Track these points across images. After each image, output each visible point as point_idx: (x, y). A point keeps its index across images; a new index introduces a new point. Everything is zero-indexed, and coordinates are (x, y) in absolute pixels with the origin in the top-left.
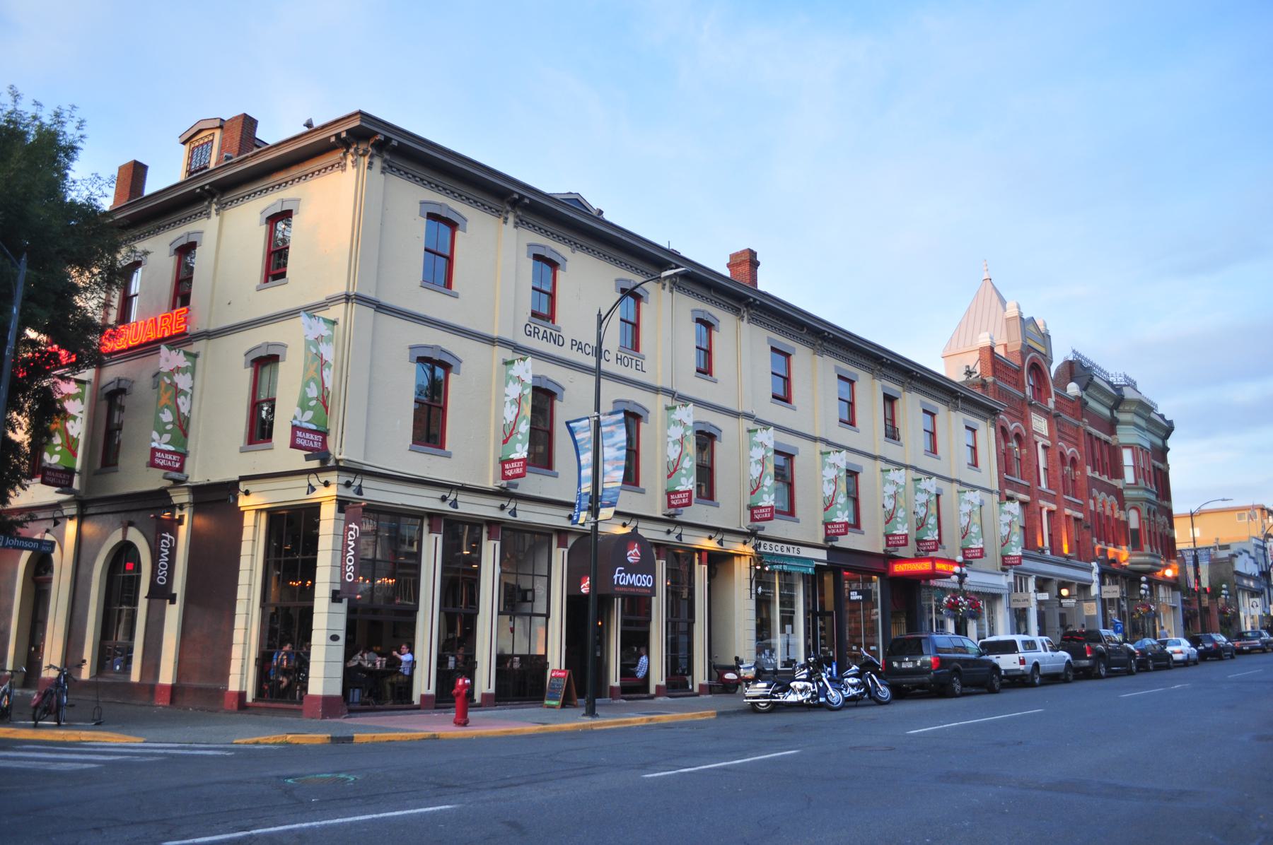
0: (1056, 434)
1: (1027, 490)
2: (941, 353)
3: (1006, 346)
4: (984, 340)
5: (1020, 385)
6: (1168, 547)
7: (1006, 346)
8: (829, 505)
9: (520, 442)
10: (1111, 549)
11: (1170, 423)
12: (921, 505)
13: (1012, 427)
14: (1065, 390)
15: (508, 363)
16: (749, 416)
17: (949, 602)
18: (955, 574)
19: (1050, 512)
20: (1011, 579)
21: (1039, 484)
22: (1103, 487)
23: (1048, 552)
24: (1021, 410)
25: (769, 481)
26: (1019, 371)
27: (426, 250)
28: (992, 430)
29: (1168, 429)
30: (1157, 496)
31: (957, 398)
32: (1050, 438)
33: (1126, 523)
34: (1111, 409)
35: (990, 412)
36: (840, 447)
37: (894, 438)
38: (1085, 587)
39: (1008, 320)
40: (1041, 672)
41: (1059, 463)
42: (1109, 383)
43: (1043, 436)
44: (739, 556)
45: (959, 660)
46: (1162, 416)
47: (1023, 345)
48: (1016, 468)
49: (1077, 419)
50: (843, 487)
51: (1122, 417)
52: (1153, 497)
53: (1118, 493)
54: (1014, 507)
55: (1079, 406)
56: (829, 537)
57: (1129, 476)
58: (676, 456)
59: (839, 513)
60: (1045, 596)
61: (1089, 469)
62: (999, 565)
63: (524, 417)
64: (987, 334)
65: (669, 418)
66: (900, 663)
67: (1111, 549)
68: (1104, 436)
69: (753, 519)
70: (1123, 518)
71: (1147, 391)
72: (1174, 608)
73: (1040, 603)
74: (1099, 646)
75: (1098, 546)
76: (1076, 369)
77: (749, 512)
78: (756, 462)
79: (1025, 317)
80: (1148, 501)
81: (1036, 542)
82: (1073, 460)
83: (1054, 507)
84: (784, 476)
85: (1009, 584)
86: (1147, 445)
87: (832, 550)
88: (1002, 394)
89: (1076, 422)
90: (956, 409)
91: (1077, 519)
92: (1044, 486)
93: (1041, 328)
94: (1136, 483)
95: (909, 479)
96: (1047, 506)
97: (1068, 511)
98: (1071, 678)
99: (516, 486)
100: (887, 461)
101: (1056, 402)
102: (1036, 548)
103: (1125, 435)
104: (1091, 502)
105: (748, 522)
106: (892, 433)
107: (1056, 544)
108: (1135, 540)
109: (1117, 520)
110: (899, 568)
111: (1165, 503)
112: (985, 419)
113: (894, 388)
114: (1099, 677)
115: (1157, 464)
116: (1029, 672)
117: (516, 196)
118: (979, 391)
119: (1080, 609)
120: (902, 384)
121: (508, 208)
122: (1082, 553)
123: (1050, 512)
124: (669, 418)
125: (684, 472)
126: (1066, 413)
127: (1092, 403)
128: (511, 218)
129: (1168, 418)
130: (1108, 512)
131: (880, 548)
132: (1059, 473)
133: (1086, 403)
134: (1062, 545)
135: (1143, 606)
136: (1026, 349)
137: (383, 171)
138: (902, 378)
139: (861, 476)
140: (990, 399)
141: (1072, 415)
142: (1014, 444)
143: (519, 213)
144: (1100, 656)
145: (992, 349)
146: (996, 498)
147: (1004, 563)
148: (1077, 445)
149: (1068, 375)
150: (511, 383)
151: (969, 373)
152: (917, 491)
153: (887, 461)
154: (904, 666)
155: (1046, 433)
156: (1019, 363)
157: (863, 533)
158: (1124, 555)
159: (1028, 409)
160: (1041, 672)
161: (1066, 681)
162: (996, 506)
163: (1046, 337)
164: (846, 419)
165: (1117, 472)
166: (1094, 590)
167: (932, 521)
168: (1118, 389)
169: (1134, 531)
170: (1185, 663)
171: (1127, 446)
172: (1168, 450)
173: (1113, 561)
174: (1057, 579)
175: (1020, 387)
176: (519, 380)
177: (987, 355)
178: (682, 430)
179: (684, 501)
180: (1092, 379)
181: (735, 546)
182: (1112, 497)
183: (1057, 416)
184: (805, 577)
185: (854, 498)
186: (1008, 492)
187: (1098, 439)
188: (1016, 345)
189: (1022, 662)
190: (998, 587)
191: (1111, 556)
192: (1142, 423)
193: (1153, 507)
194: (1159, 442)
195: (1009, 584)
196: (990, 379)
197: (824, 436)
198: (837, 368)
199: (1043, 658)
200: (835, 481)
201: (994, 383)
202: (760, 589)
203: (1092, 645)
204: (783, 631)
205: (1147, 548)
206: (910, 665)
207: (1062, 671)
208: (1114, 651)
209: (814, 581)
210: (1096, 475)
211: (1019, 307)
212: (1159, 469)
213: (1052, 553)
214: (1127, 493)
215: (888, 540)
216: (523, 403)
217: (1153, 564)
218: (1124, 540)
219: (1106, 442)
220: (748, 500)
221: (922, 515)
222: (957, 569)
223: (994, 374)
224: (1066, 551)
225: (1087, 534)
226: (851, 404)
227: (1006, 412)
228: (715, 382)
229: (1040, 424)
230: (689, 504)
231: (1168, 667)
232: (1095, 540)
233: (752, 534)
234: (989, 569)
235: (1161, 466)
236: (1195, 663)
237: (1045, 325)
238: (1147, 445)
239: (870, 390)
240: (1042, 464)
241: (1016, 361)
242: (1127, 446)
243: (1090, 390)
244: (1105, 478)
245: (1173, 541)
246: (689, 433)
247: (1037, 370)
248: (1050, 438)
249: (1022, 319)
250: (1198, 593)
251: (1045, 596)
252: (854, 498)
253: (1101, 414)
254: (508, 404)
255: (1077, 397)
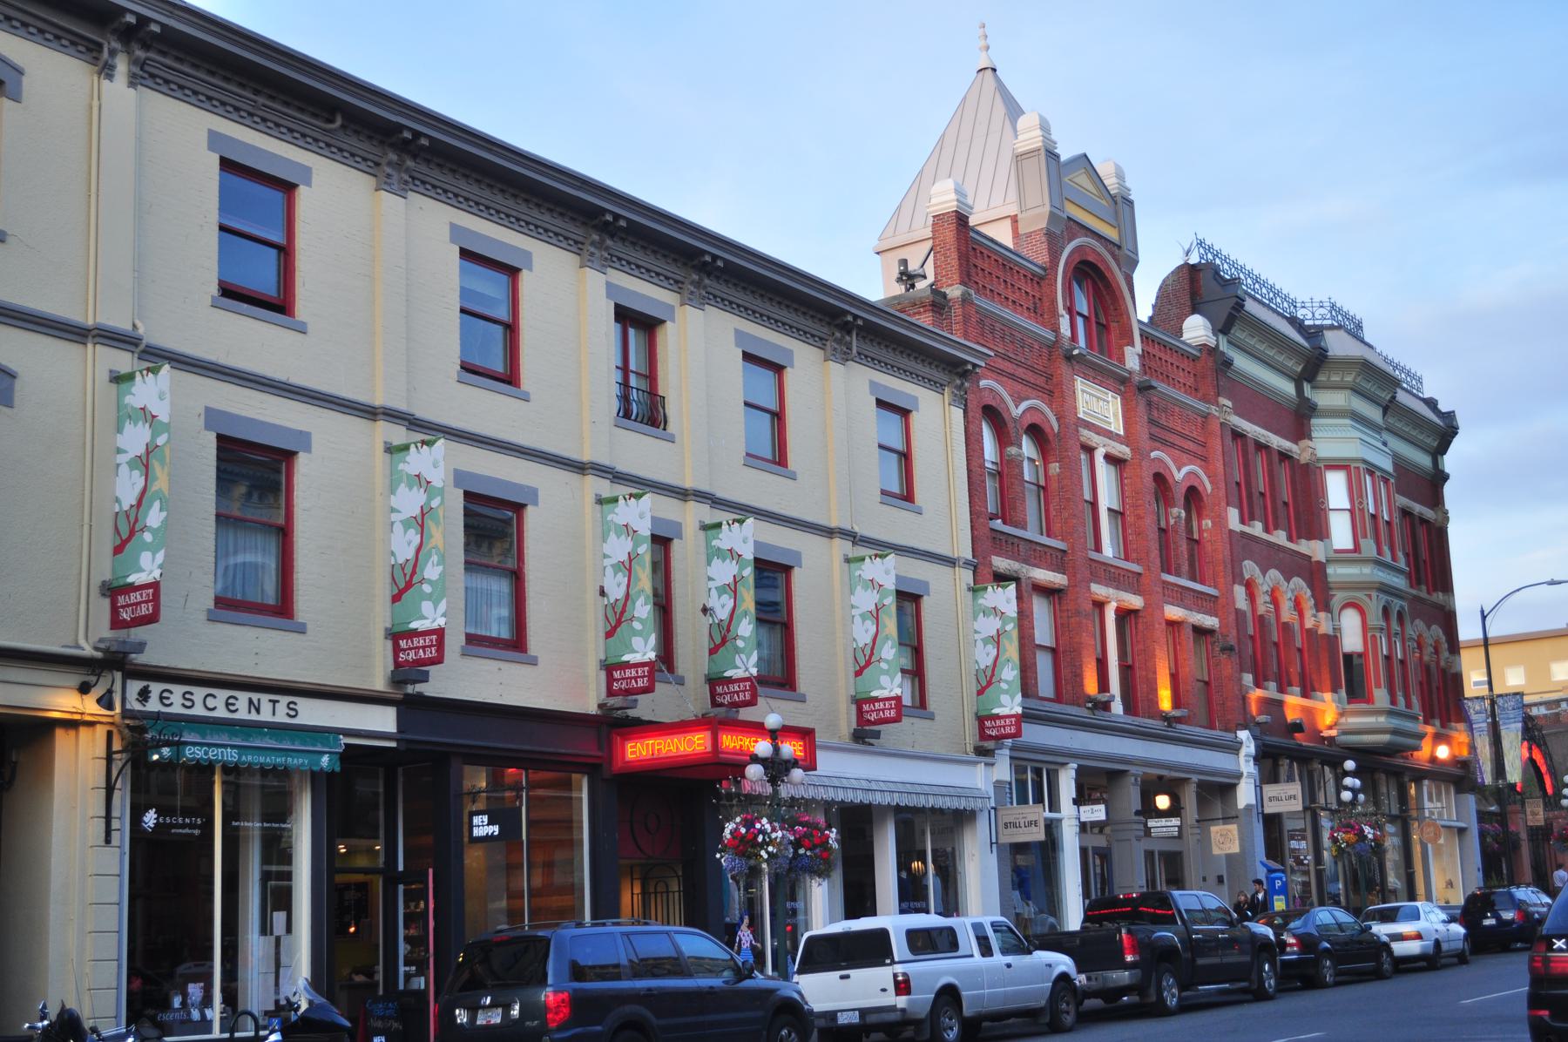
0: (1143, 431)
1: (1058, 561)
2: (873, 242)
3: (1014, 220)
4: (943, 198)
5: (1042, 310)
6: (1442, 697)
7: (1014, 220)
8: (864, 663)
9: (1006, 692)
10: (1294, 702)
11: (1449, 417)
12: (721, 590)
13: (1017, 411)
14: (1180, 332)
15: (120, 379)
16: (393, 415)
17: (734, 832)
18: (755, 759)
19: (1124, 615)
20: (1003, 770)
21: (1098, 548)
22: (1270, 556)
23: (1117, 707)
24: (1048, 371)
25: (746, 628)
26: (1041, 279)
27: (463, 311)
28: (958, 414)
29: (1444, 432)
30: (1409, 576)
31: (847, 328)
32: (1127, 439)
33: (1333, 640)
34: (1298, 381)
35: (949, 370)
36: (744, 511)
37: (779, 464)
38: (1218, 790)
39: (1019, 158)
40: (968, 1011)
41: (1150, 498)
42: (1294, 321)
43: (1109, 434)
44: (72, 725)
45: (648, 997)
46: (1431, 403)
47: (1053, 217)
48: (1031, 508)
49: (1205, 399)
50: (890, 625)
51: (1323, 399)
52: (1400, 582)
53: (1314, 573)
54: (1004, 598)
55: (1212, 369)
56: (405, 673)
57: (1341, 533)
58: (990, 662)
59: (884, 680)
60: (1097, 813)
61: (1233, 515)
62: (971, 736)
63: (746, 614)
64: (949, 184)
65: (119, 406)
66: (473, 1009)
67: (1294, 702)
68: (1277, 442)
69: (117, 623)
70: (1325, 628)
71: (1389, 340)
72: (1461, 831)
73: (1084, 827)
74: (1165, 933)
75: (1256, 694)
76: (1201, 285)
77: (854, 707)
78: (985, 641)
79: (1065, 153)
80: (1384, 589)
81: (1082, 685)
82: (1193, 496)
83: (1136, 602)
84: (775, 617)
85: (998, 785)
86: (1387, 464)
87: (412, 707)
88: (985, 326)
89: (1202, 406)
90: (845, 358)
91: (1200, 631)
92: (1108, 551)
93: (1111, 182)
94: (1357, 549)
95: (590, 499)
96: (1116, 598)
97: (1173, 612)
98: (1069, 1019)
99: (140, 647)
100: (617, 477)
101: (1144, 356)
102: (1080, 699)
103: (1333, 440)
104: (1240, 592)
105: (106, 633)
106: (643, 407)
107: (1141, 689)
108: (1352, 678)
109: (1311, 634)
110: (638, 750)
111: (1439, 597)
112: (937, 386)
113: (648, 293)
114: (1157, 1010)
115: (1417, 508)
116: (923, 1012)
117: (131, 19)
118: (925, 320)
119: (1205, 841)
120: (677, 285)
121: (116, 45)
122: (1211, 710)
123: (1124, 615)
124: (119, 406)
125: (1004, 686)
126: (1167, 379)
127: (1242, 362)
128: (122, 66)
129: (1443, 407)
130: (1287, 614)
131: (588, 699)
132: (1149, 524)
133: (1228, 363)
134: (1153, 690)
135: (1348, 827)
136: (1062, 229)
137: (134, 81)
138: (577, 231)
139: (926, 603)
140: (955, 339)
141: (1194, 391)
142: (1027, 448)
143: (140, 54)
144: (1158, 958)
145: (961, 219)
146: (967, 576)
147: (983, 736)
148: (1204, 460)
149: (1186, 299)
150: (612, 536)
151: (908, 278)
152: (714, 554)
153: (617, 477)
154: (481, 1020)
155: (1118, 427)
156: (1042, 258)
157: (533, 662)
158: (1329, 712)
159: (1064, 369)
160: (968, 1011)
161: (1056, 1028)
162: (965, 597)
163: (1121, 206)
164: (896, 489)
165: (1312, 522)
166: (1245, 795)
167: (643, 609)
168: (1313, 333)
169: (1348, 658)
170: (1434, 960)
171: (1335, 465)
172: (1445, 477)
173: (1297, 727)
174: (1140, 770)
175: (1022, 307)
176: (627, 529)
177: (949, 234)
178: (997, 623)
179: (145, 610)
180: (1239, 305)
181: (63, 701)
182: (1297, 581)
183: (1145, 388)
184: (318, 779)
185: (913, 644)
186: (1001, 563)
187: (1261, 447)
188: (1037, 219)
189: (903, 987)
190: (960, 792)
191: (1291, 716)
192: (1374, 414)
193: (1397, 604)
194: (1424, 460)
195: (998, 785)
196: (954, 292)
197: (704, 487)
198: (874, 386)
199: (976, 972)
200: (876, 615)
201: (965, 300)
202: (150, 818)
203: (1142, 929)
204: (265, 929)
205: (1381, 696)
206: (496, 1018)
207: (923, 1016)
208: (1210, 944)
209: (356, 786)
210: (1257, 529)
211: (1045, 127)
212: (1424, 521)
213: (1130, 707)
214: (1335, 572)
215: (982, 728)
216: (740, 588)
217: (1395, 732)
218: (1328, 683)
219: (1285, 456)
220: (104, 570)
221: (723, 614)
222: (763, 747)
223: (966, 279)
224: (1166, 704)
225: (1228, 666)
226: (905, 457)
227: (999, 373)
228: (302, 330)
229: (1099, 406)
230: (438, 660)
231: (1377, 975)
232: (1248, 679)
233: (111, 664)
234: (939, 750)
235: (1429, 514)
236: (1461, 959)
237: (1120, 176)
238: (1387, 464)
239: (566, 297)
240: (1107, 498)
241: (1038, 255)
242: (1335, 465)
243: (1238, 333)
244: (1280, 537)
245: (1457, 680)
246: (1009, 627)
247: (1100, 278)
248: (1127, 439)
249: (1052, 155)
250: (1505, 795)
251: (1097, 813)
252: (913, 644)
253: (1416, 466)
254: (124, 469)
255: (1203, 347)
